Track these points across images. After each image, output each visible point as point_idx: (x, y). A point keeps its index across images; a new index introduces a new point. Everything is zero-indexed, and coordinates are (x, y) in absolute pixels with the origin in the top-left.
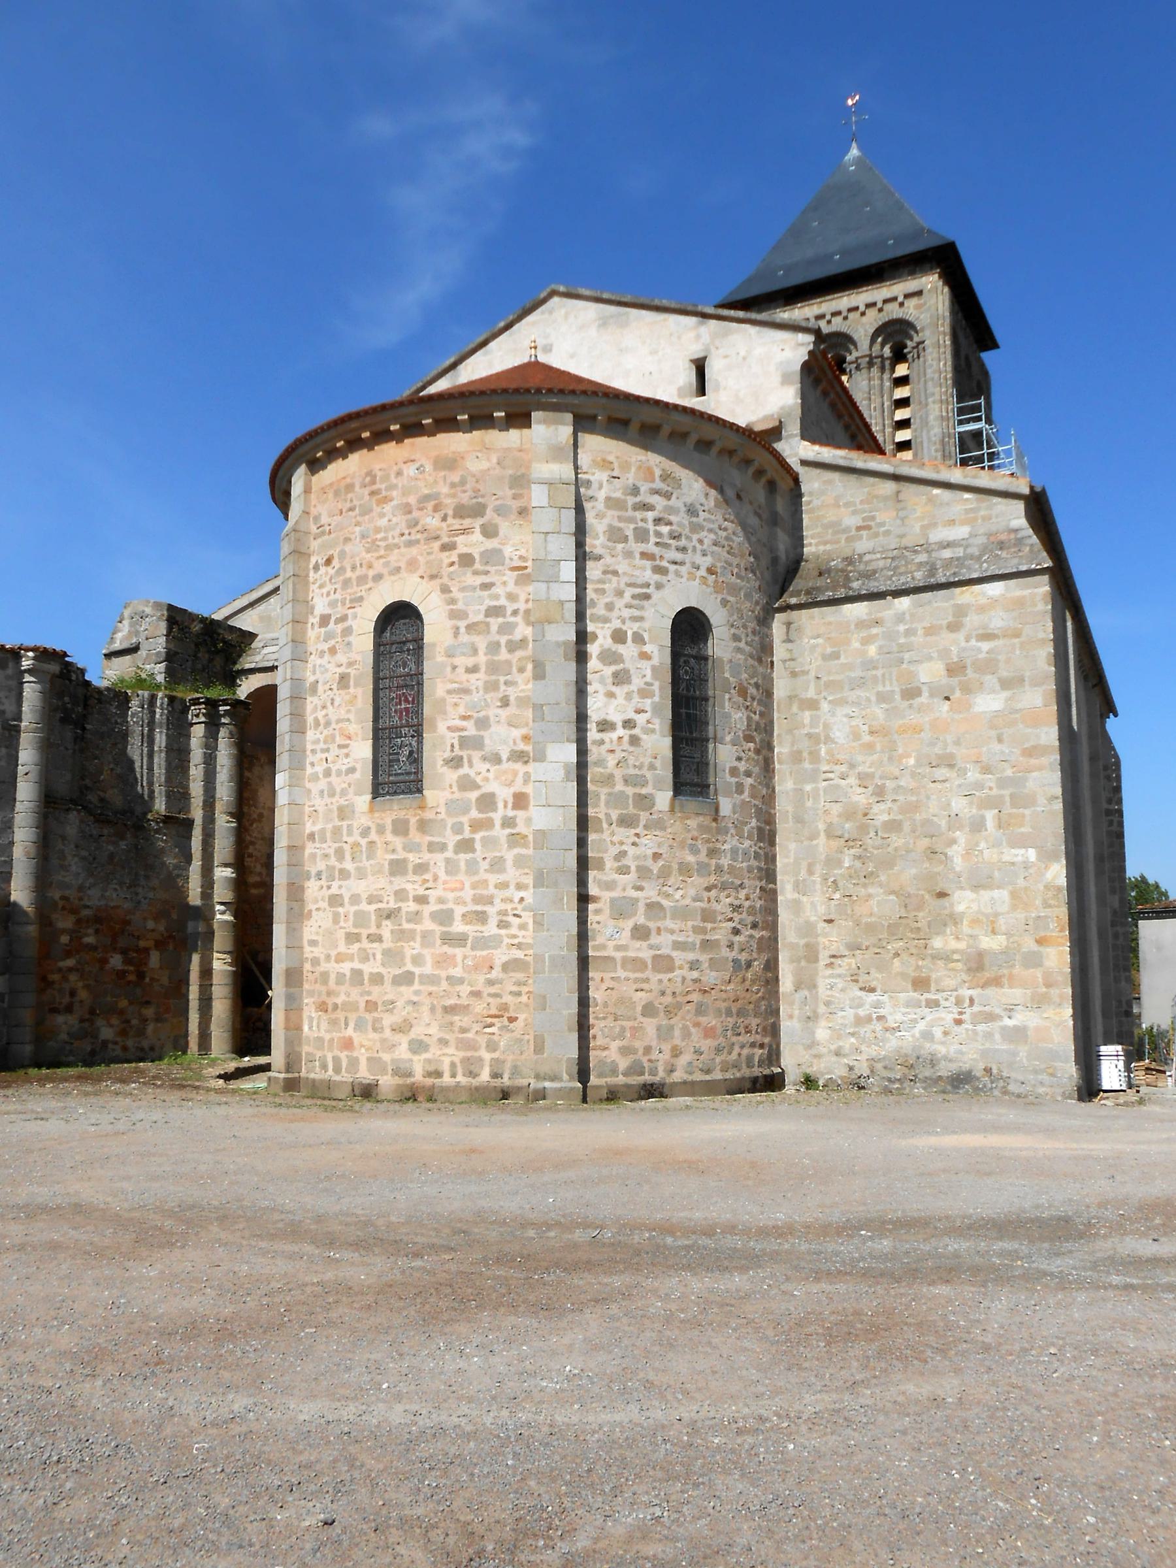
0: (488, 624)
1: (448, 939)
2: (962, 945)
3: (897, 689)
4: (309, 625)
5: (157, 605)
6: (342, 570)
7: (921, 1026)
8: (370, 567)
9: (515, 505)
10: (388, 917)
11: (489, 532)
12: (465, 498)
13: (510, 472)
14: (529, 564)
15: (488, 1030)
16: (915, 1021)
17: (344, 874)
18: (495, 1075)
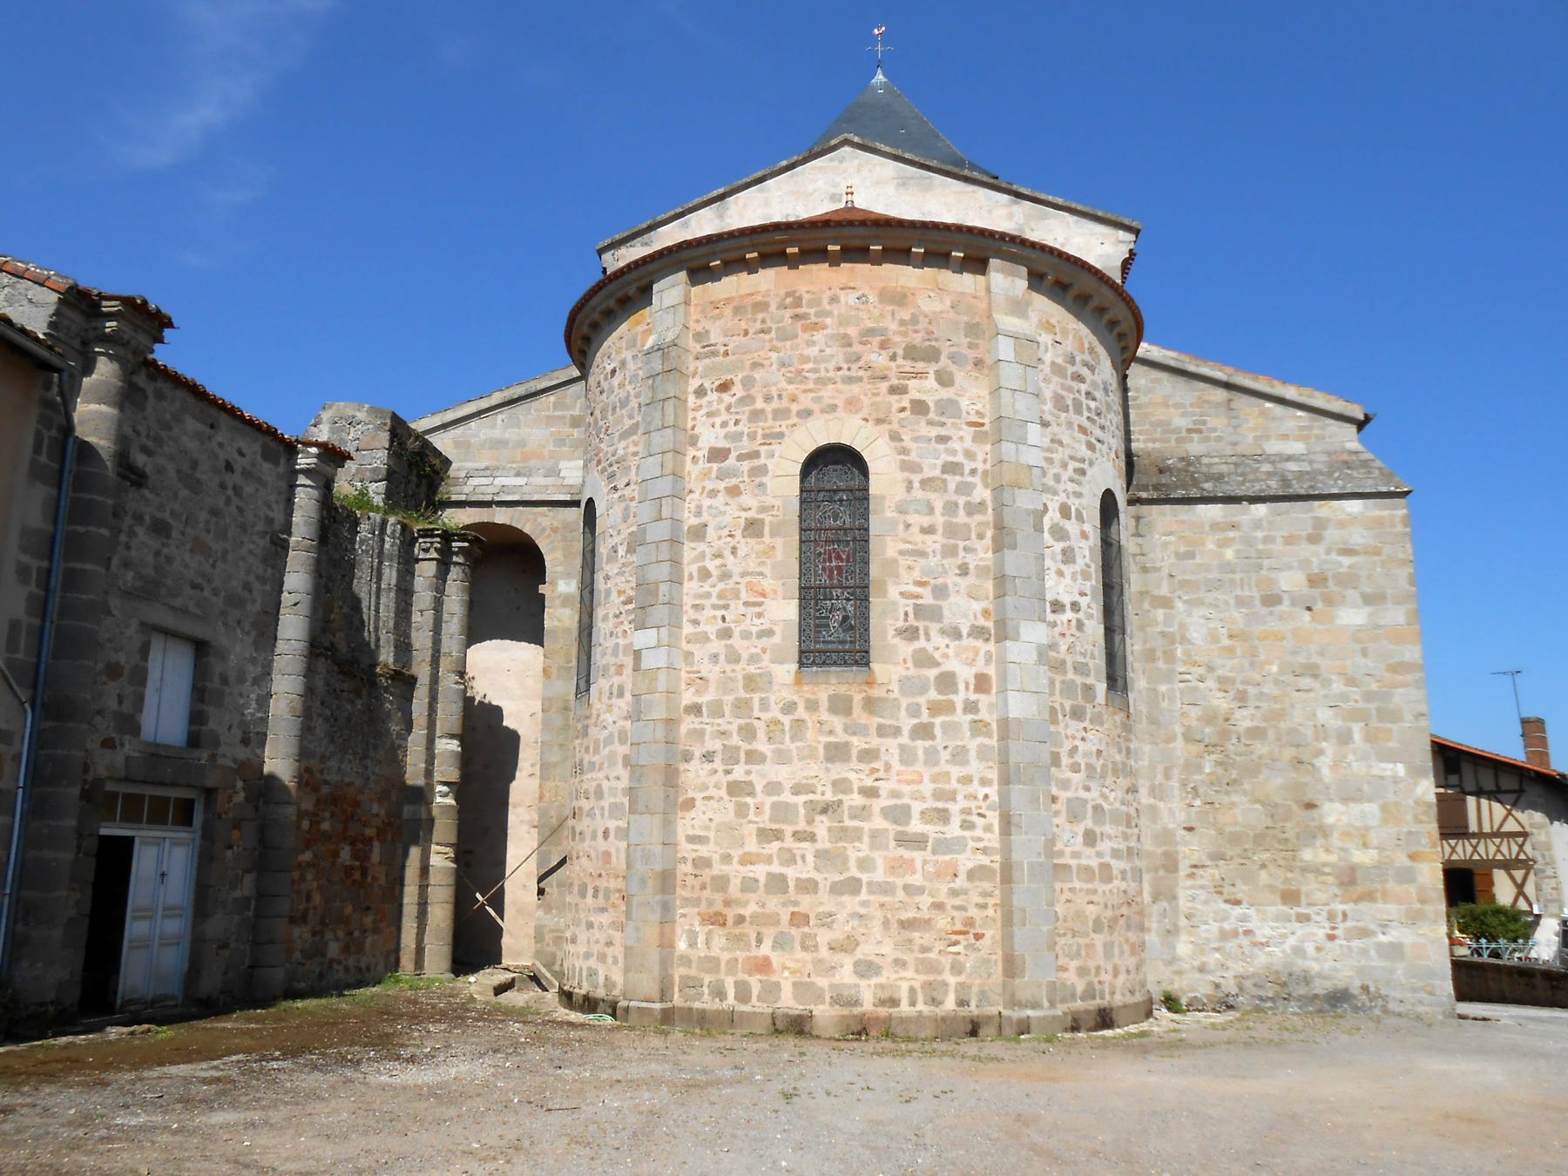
0: (944, 481)
1: (903, 840)
2: (1333, 858)
3: (1257, 595)
4: (689, 458)
5: (375, 411)
6: (747, 399)
7: (1292, 941)
8: (794, 400)
9: (971, 355)
10: (824, 811)
11: (944, 380)
12: (917, 339)
13: (965, 318)
14: (986, 421)
15: (952, 949)
16: (1283, 936)
17: (754, 757)
18: (962, 1003)
